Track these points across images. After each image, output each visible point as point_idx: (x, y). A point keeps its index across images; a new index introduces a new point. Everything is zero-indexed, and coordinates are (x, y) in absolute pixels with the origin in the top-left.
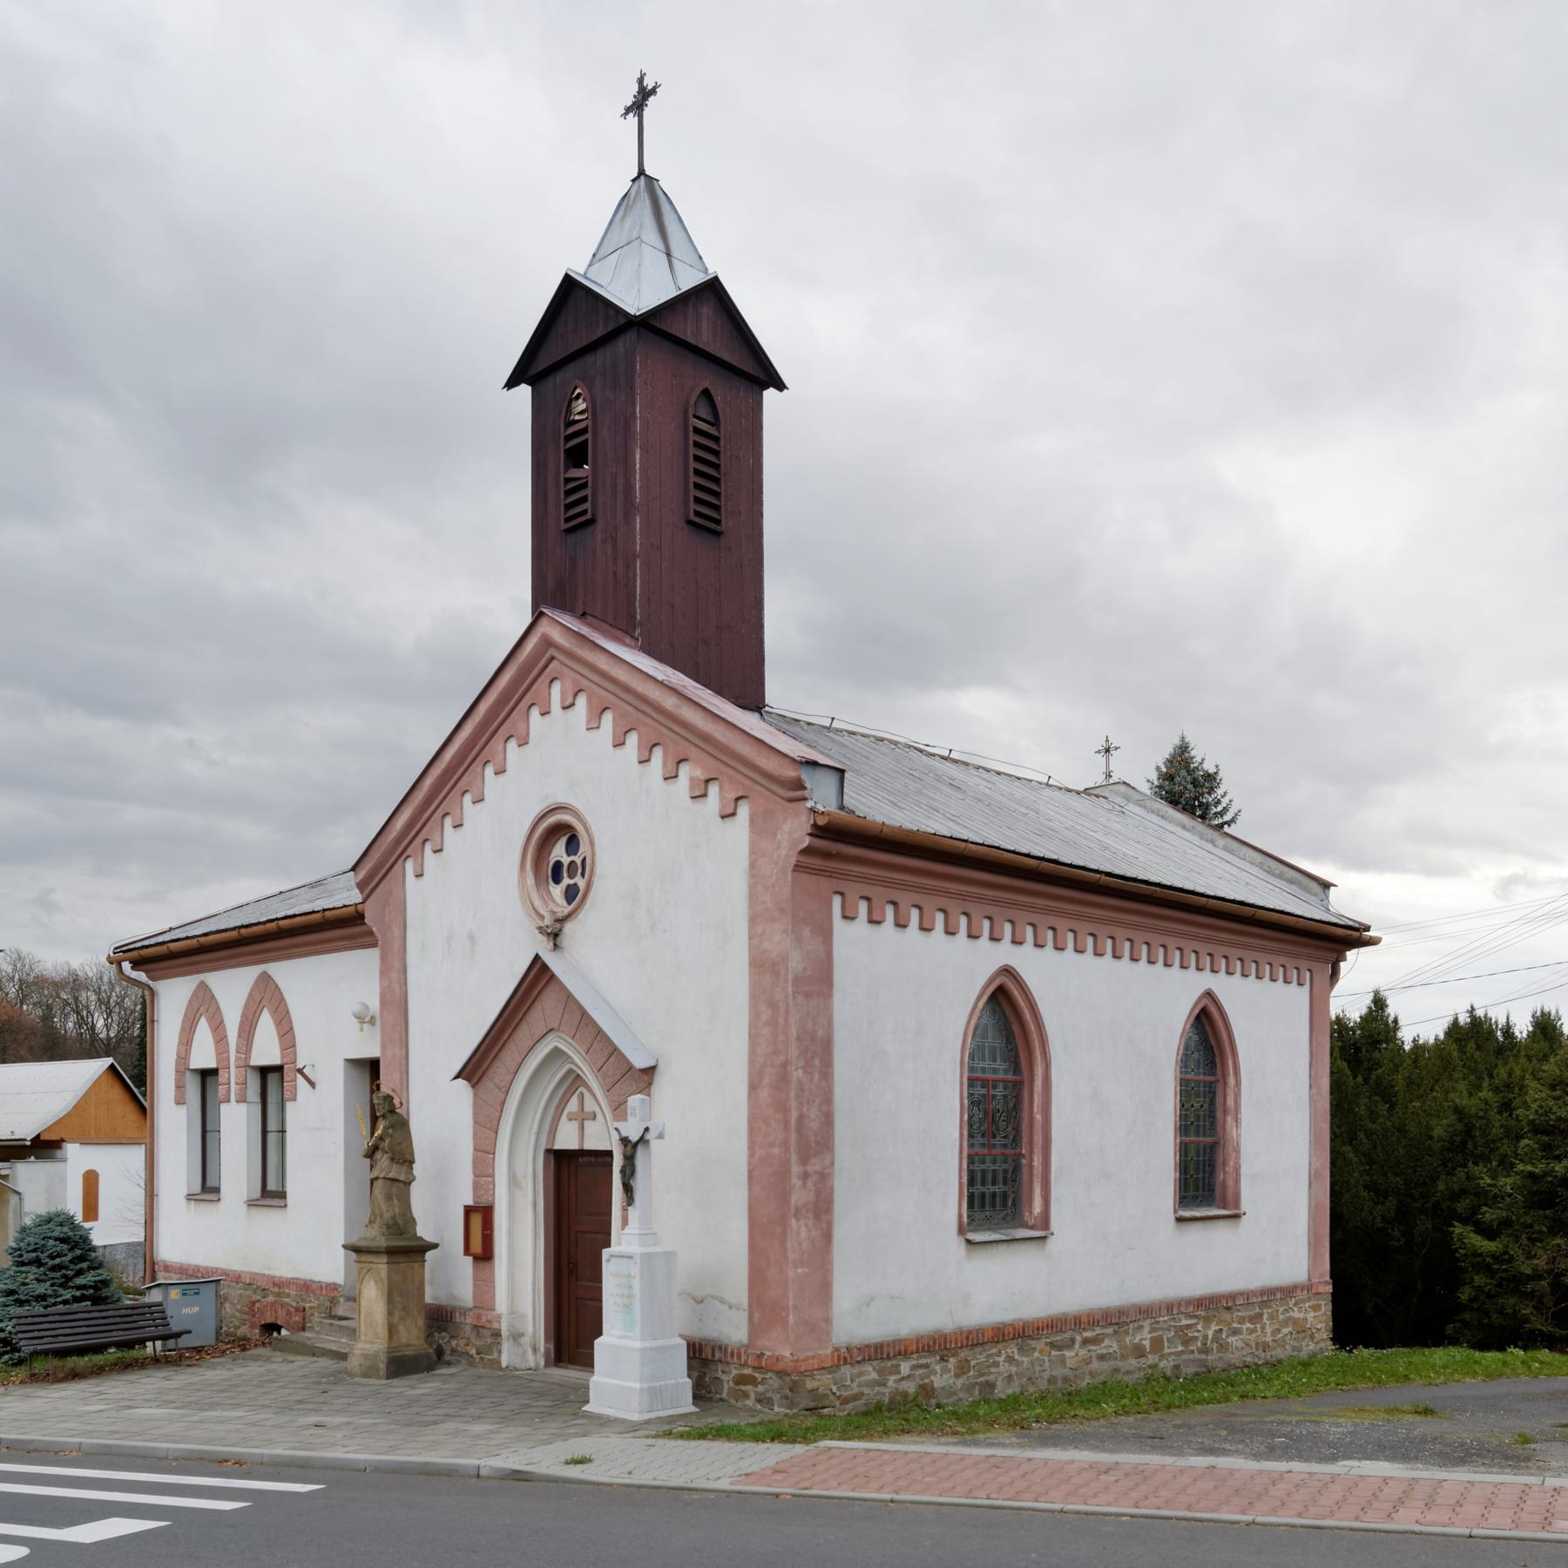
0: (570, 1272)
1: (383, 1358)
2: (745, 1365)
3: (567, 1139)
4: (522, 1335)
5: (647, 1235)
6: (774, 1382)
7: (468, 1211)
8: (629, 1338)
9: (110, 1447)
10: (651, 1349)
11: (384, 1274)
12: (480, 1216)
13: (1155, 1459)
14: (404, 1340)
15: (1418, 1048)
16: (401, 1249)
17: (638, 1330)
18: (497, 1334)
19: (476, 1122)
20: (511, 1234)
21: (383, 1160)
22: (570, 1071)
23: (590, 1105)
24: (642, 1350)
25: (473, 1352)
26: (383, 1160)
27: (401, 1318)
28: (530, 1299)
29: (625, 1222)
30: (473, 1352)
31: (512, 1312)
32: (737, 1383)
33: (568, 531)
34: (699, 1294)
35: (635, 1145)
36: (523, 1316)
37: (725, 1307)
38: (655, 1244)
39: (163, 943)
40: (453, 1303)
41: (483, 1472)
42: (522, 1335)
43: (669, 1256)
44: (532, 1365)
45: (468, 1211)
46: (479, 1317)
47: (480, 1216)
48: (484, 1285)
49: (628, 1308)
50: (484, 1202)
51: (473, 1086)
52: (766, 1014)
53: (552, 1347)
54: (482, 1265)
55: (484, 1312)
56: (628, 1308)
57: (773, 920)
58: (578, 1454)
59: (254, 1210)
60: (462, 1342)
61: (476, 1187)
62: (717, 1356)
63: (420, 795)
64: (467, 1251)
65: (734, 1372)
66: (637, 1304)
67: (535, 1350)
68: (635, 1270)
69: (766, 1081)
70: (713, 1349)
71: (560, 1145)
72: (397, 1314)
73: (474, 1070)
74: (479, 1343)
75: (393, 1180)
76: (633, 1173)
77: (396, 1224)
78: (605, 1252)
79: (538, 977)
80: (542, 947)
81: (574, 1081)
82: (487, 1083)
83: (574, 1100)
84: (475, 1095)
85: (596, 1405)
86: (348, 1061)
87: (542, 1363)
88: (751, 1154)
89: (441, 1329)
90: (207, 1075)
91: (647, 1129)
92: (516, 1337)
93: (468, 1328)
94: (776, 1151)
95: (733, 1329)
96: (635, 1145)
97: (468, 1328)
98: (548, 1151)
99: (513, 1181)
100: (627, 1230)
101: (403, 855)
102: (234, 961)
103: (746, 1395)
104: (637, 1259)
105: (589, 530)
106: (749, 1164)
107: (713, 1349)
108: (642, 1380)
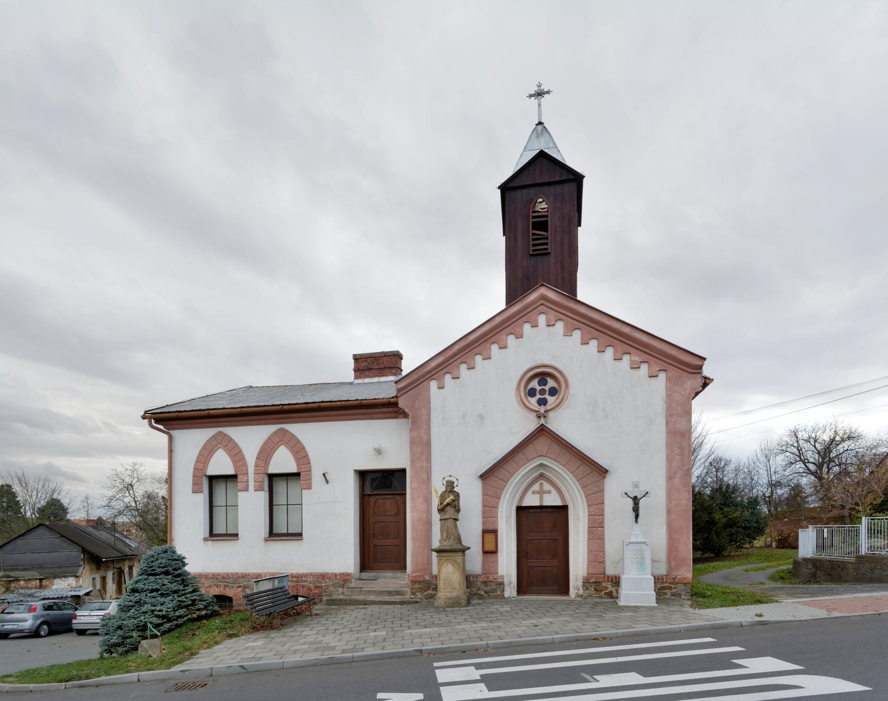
2: (666, 582)
6: (682, 587)
9: (511, 643)
12: (490, 532)
13: (816, 599)
15: (69, 520)
25: (483, 593)
33: (532, 255)
39: (169, 412)
41: (744, 624)
52: (677, 451)
57: (682, 417)
58: (759, 613)
63: (450, 353)
69: (678, 476)
71: (526, 503)
74: (486, 589)
85: (622, 602)
86: (355, 471)
93: (479, 583)
94: (684, 502)
102: (366, 416)
103: (665, 594)
105: (545, 258)
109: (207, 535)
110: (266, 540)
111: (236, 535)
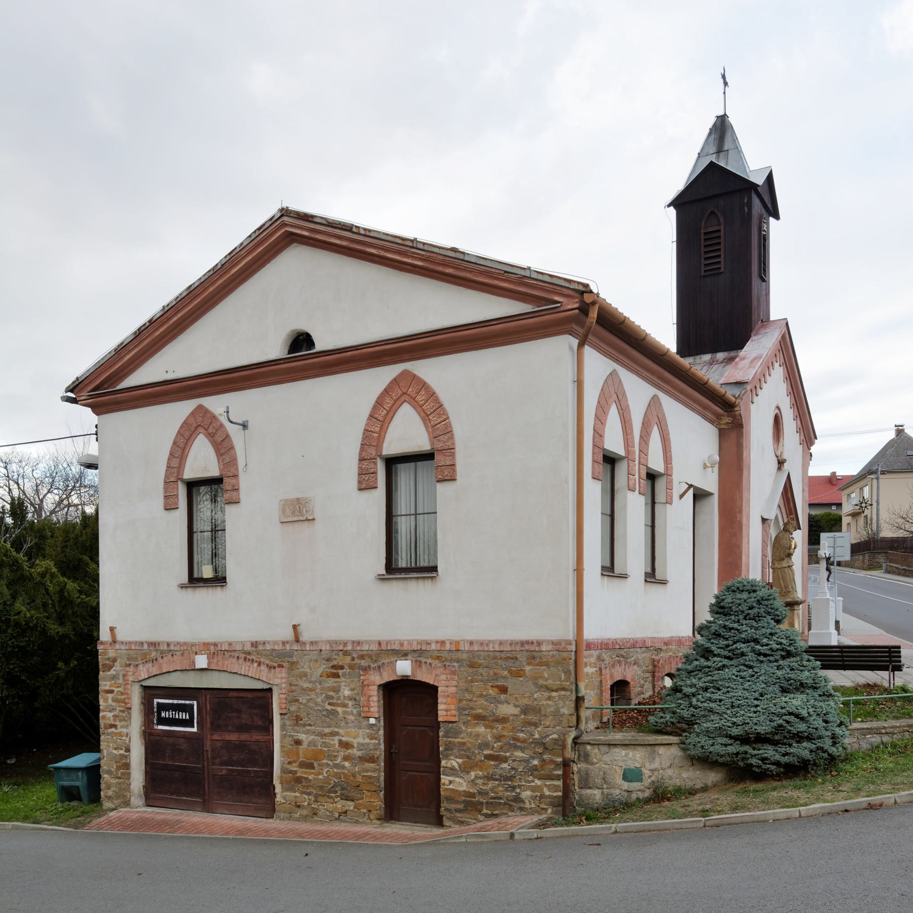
109: (185, 579)
110: (381, 578)
111: (434, 569)
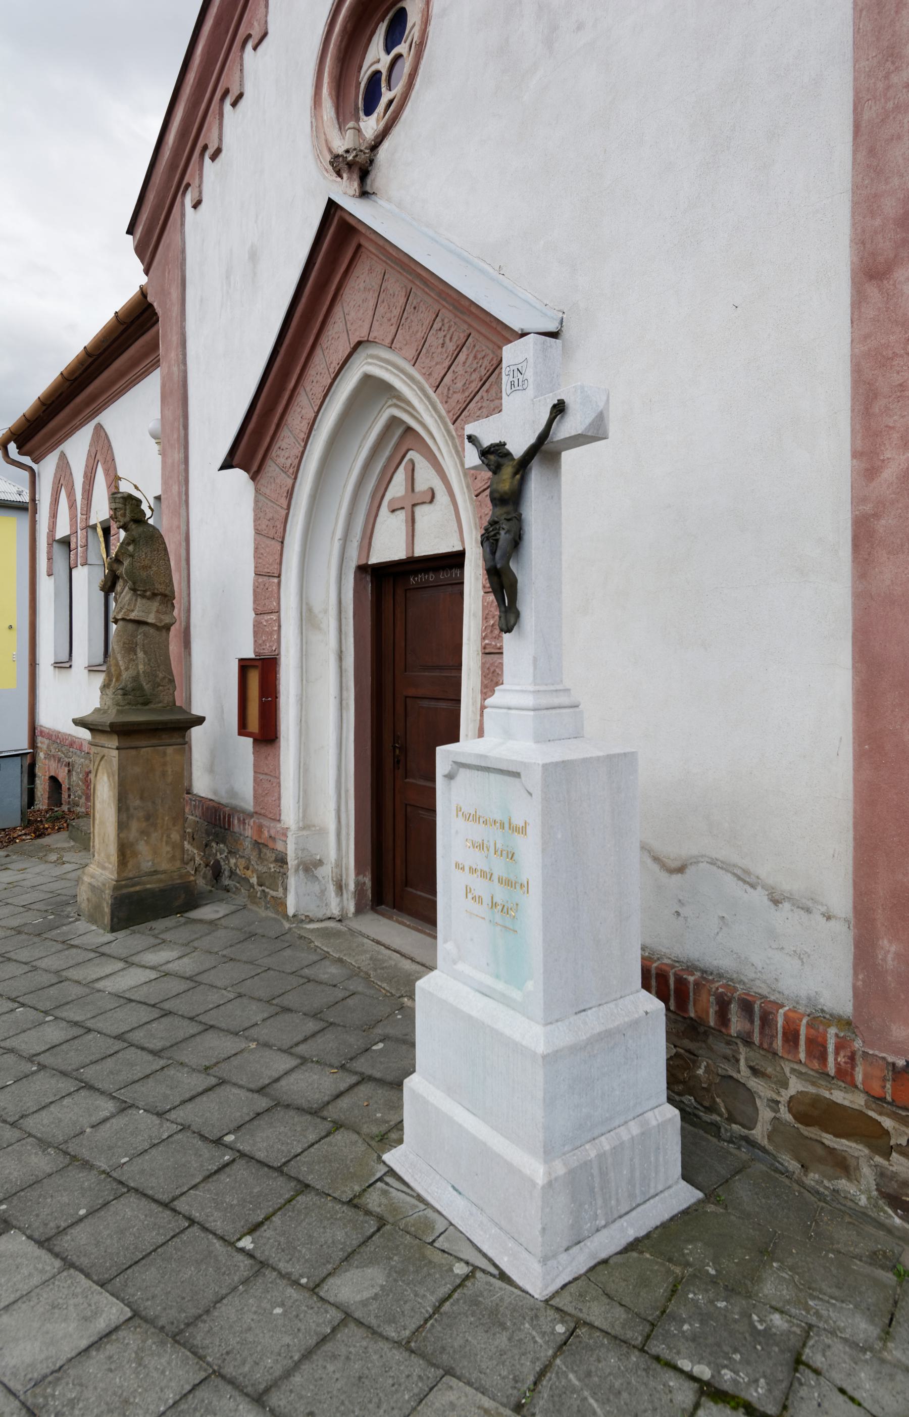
0: (397, 762)
1: (107, 895)
2: (844, 1076)
3: (389, 547)
4: (320, 863)
5: (557, 710)
7: (245, 666)
8: (505, 1001)
10: (574, 1049)
11: (115, 762)
12: (259, 676)
14: (146, 865)
16: (149, 720)
17: (534, 985)
18: (282, 860)
19: (258, 532)
20: (303, 701)
21: (123, 591)
22: (394, 421)
23: (426, 477)
24: (551, 1059)
25: (254, 880)
26: (123, 591)
27: (144, 833)
28: (332, 805)
29: (492, 679)
30: (254, 880)
31: (306, 826)
32: (803, 1118)
34: (673, 851)
35: (524, 464)
36: (322, 832)
37: (759, 897)
38: (577, 735)
40: (234, 802)
42: (320, 863)
43: (619, 765)
44: (335, 911)
45: (245, 666)
46: (260, 828)
47: (259, 676)
48: (267, 779)
49: (505, 913)
50: (267, 652)
51: (253, 478)
53: (367, 880)
54: (265, 750)
55: (265, 822)
56: (505, 913)
59: (92, 673)
60: (242, 863)
61: (258, 630)
62: (737, 1023)
64: (243, 729)
65: (795, 1086)
66: (532, 907)
67: (340, 887)
68: (527, 810)
70: (723, 1005)
72: (135, 826)
73: (249, 450)
75: (139, 623)
76: (517, 541)
77: (140, 688)
78: (444, 755)
79: (339, 243)
80: (343, 192)
81: (402, 438)
82: (271, 469)
83: (400, 477)
84: (257, 490)
87: (352, 908)
88: (867, 459)
89: (221, 838)
90: (66, 542)
91: (559, 409)
92: (310, 867)
93: (247, 844)
95: (806, 964)
96: (524, 464)
97: (247, 844)
98: (362, 569)
99: (308, 618)
100: (498, 697)
101: (181, 187)
102: (76, 421)
104: (534, 780)
106: (858, 500)
107: (723, 1005)
108: (548, 1153)
